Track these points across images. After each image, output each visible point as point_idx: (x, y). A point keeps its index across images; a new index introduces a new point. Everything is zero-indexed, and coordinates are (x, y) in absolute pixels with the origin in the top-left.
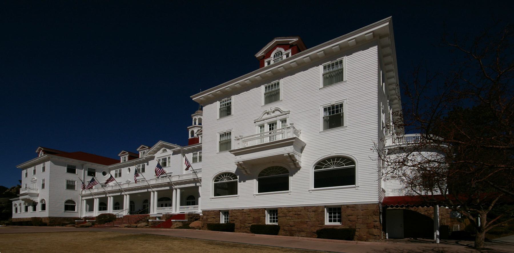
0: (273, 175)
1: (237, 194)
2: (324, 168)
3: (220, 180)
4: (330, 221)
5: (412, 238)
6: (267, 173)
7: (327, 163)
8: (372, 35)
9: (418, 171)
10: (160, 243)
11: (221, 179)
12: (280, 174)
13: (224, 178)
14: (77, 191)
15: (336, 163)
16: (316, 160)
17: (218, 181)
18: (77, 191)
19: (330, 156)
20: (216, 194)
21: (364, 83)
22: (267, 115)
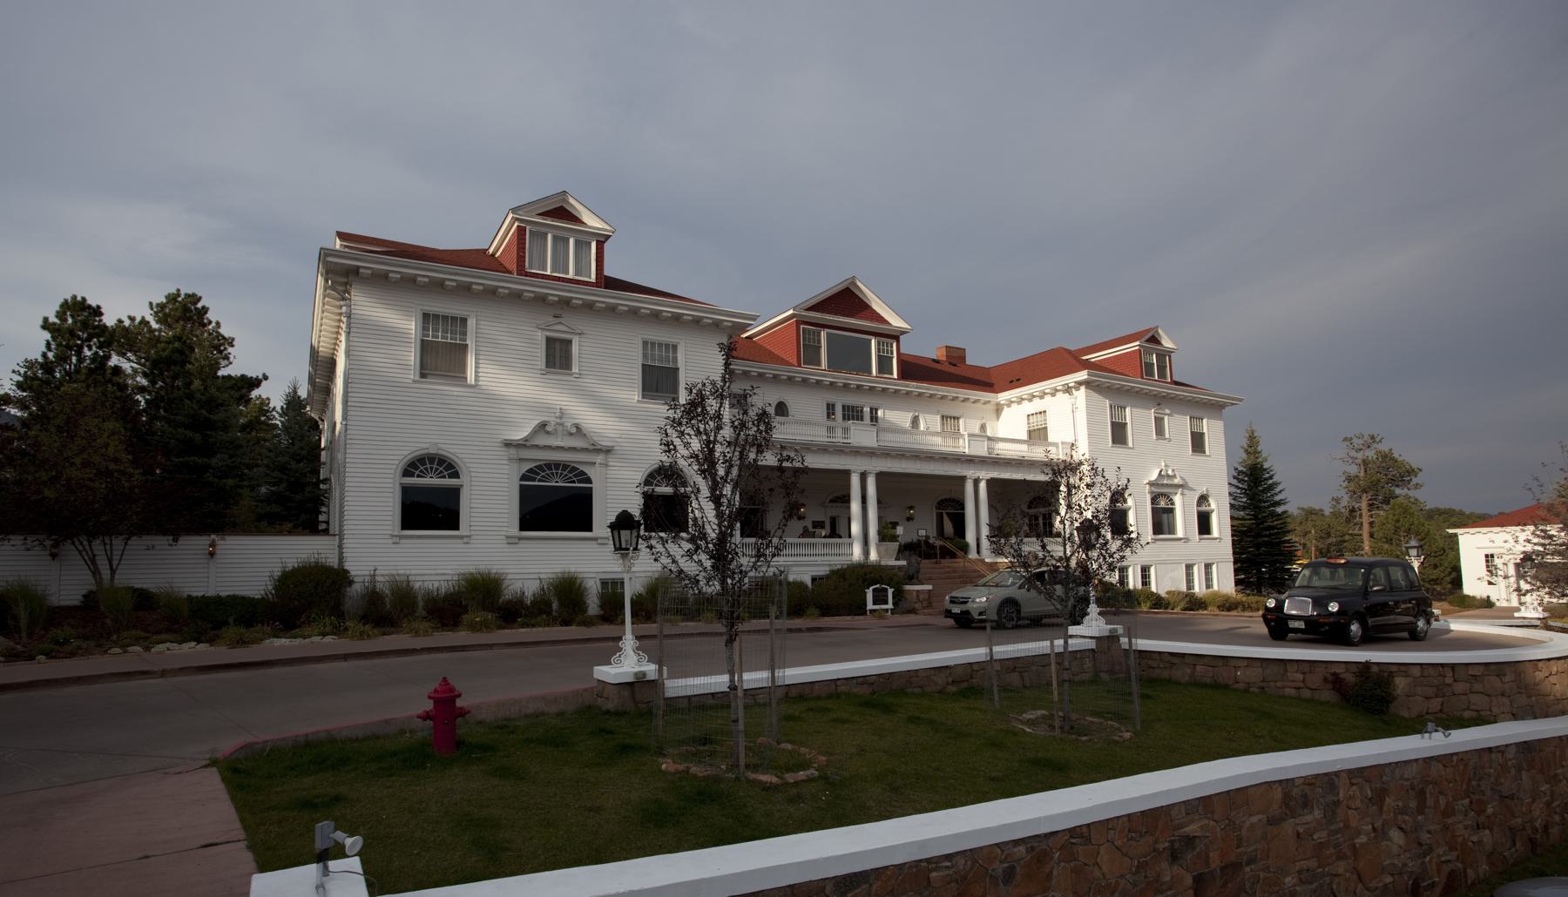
0: (557, 482)
1: (457, 527)
2: (539, 481)
3: (417, 472)
4: (886, 603)
5: (1342, 621)
6: (543, 476)
7: (544, 471)
8: (1096, 397)
9: (1401, 547)
10: (1176, 834)
11: (421, 471)
12: (574, 482)
13: (431, 468)
14: (1132, 448)
15: (566, 475)
16: (407, 456)
17: (534, 480)
18: (1132, 448)
19: (426, 451)
20: (526, 524)
21: (510, 360)
22: (66, 298)
